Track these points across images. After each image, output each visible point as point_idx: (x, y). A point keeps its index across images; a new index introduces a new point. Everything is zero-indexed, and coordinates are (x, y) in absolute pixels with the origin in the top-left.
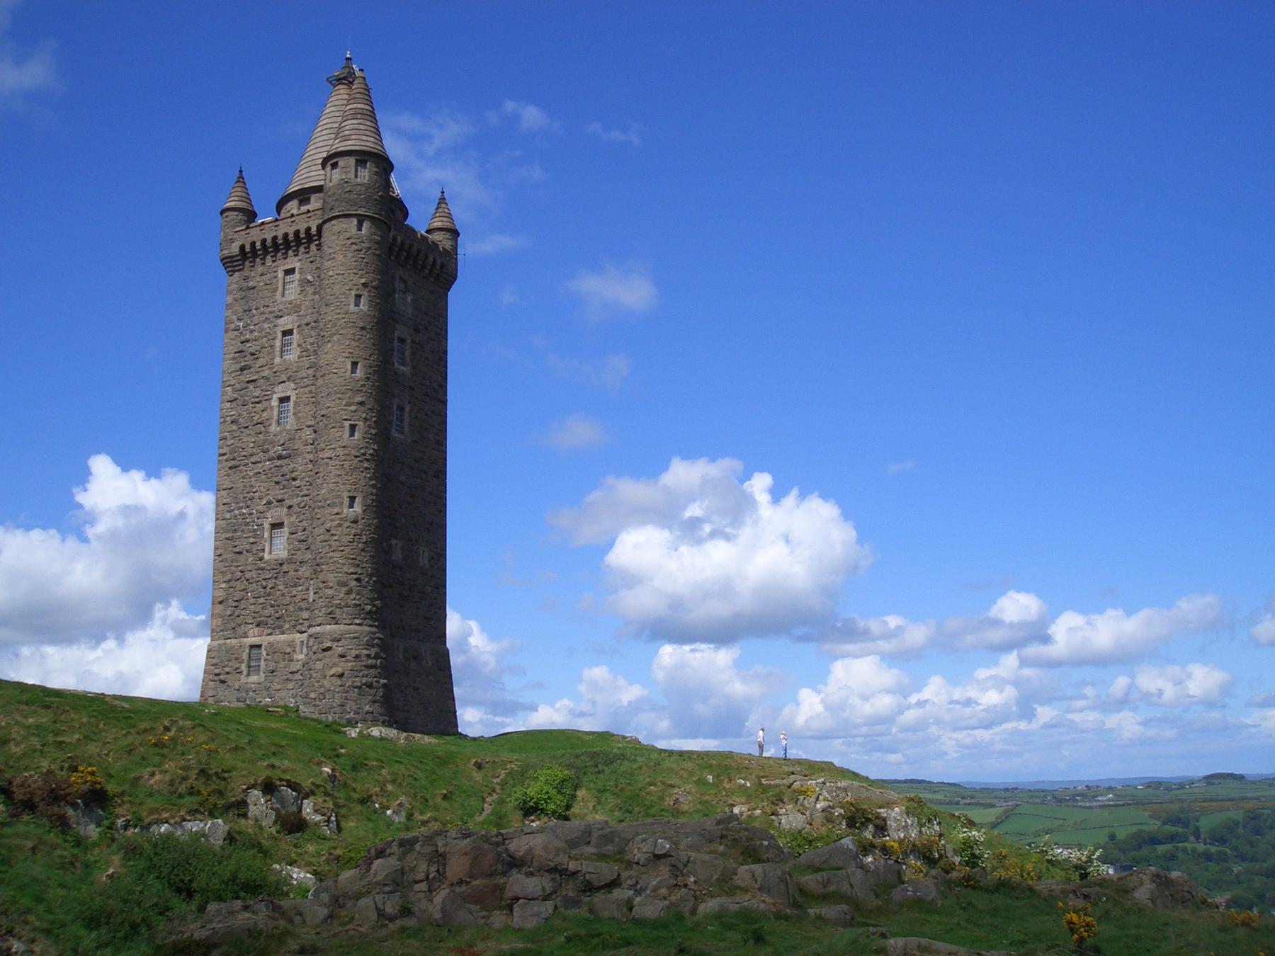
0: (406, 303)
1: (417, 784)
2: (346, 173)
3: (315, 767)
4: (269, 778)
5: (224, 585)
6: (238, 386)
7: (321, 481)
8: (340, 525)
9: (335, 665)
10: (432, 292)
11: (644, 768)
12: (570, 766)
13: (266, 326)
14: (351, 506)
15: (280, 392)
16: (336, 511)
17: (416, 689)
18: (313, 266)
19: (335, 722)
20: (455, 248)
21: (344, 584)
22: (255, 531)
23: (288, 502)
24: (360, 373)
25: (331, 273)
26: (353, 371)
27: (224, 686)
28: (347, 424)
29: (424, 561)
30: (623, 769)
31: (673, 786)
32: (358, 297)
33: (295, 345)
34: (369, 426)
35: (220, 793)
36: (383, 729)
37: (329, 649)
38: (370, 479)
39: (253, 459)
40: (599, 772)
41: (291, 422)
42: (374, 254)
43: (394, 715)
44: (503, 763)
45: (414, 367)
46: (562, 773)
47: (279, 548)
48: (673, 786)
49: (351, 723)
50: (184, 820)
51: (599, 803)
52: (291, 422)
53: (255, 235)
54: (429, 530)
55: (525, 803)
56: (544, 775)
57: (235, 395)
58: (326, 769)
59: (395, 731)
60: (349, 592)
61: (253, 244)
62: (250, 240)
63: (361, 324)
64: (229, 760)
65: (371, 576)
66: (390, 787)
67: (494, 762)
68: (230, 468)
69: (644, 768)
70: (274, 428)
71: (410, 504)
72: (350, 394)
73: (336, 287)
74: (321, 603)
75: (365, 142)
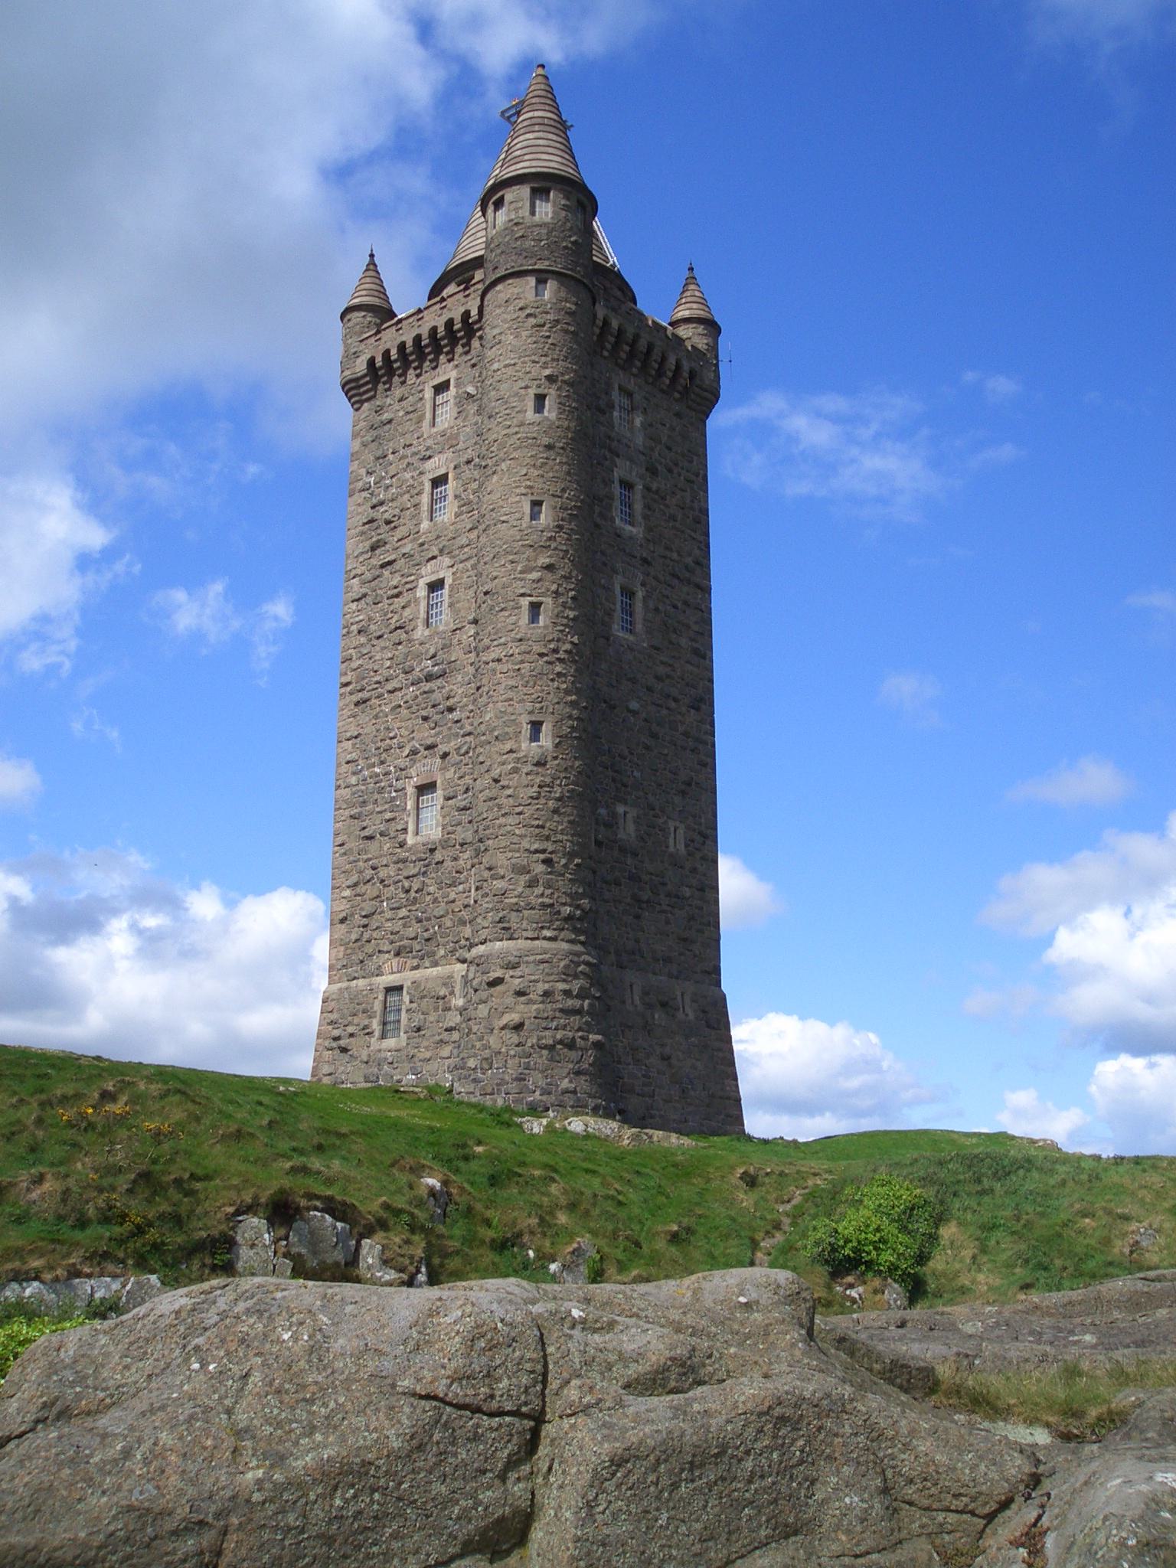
0: (632, 427)
1: (622, 1214)
2: (516, 210)
3: (403, 1178)
4: (282, 1191)
5: (347, 893)
6: (368, 576)
7: (484, 699)
8: (515, 770)
9: (509, 1009)
10: (678, 415)
11: (1071, 1184)
12: (926, 1181)
13: (407, 475)
14: (535, 736)
15: (429, 573)
16: (508, 747)
17: (666, 1058)
18: (476, 372)
19: (507, 1109)
20: (714, 348)
21: (524, 870)
22: (393, 799)
23: (442, 748)
24: (545, 518)
25: (496, 366)
26: (534, 516)
27: (345, 1057)
28: (525, 602)
29: (677, 844)
30: (1029, 1186)
31: (1126, 1218)
32: (540, 399)
33: (450, 498)
34: (564, 605)
35: (177, 1221)
36: (591, 1121)
37: (494, 983)
38: (567, 692)
39: (390, 686)
40: (983, 1193)
41: (445, 619)
42: (566, 332)
43: (614, 1095)
44: (801, 1176)
45: (649, 529)
46: (906, 1193)
47: (430, 823)
48: (1126, 1218)
49: (535, 1110)
50: (78, 1274)
51: (984, 1250)
52: (445, 619)
53: (390, 339)
54: (683, 793)
55: (834, 1249)
56: (874, 1196)
57: (364, 590)
58: (431, 1181)
59: (614, 1125)
60: (532, 884)
62: (382, 348)
63: (546, 441)
64: (215, 1155)
65: (571, 855)
66: (562, 1218)
67: (781, 1174)
68: (357, 704)
69: (1071, 1184)
70: (421, 632)
71: (647, 748)
72: (529, 552)
73: (504, 387)
74: (486, 904)
75: (550, 162)
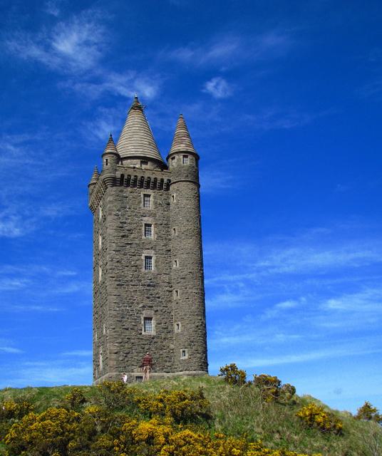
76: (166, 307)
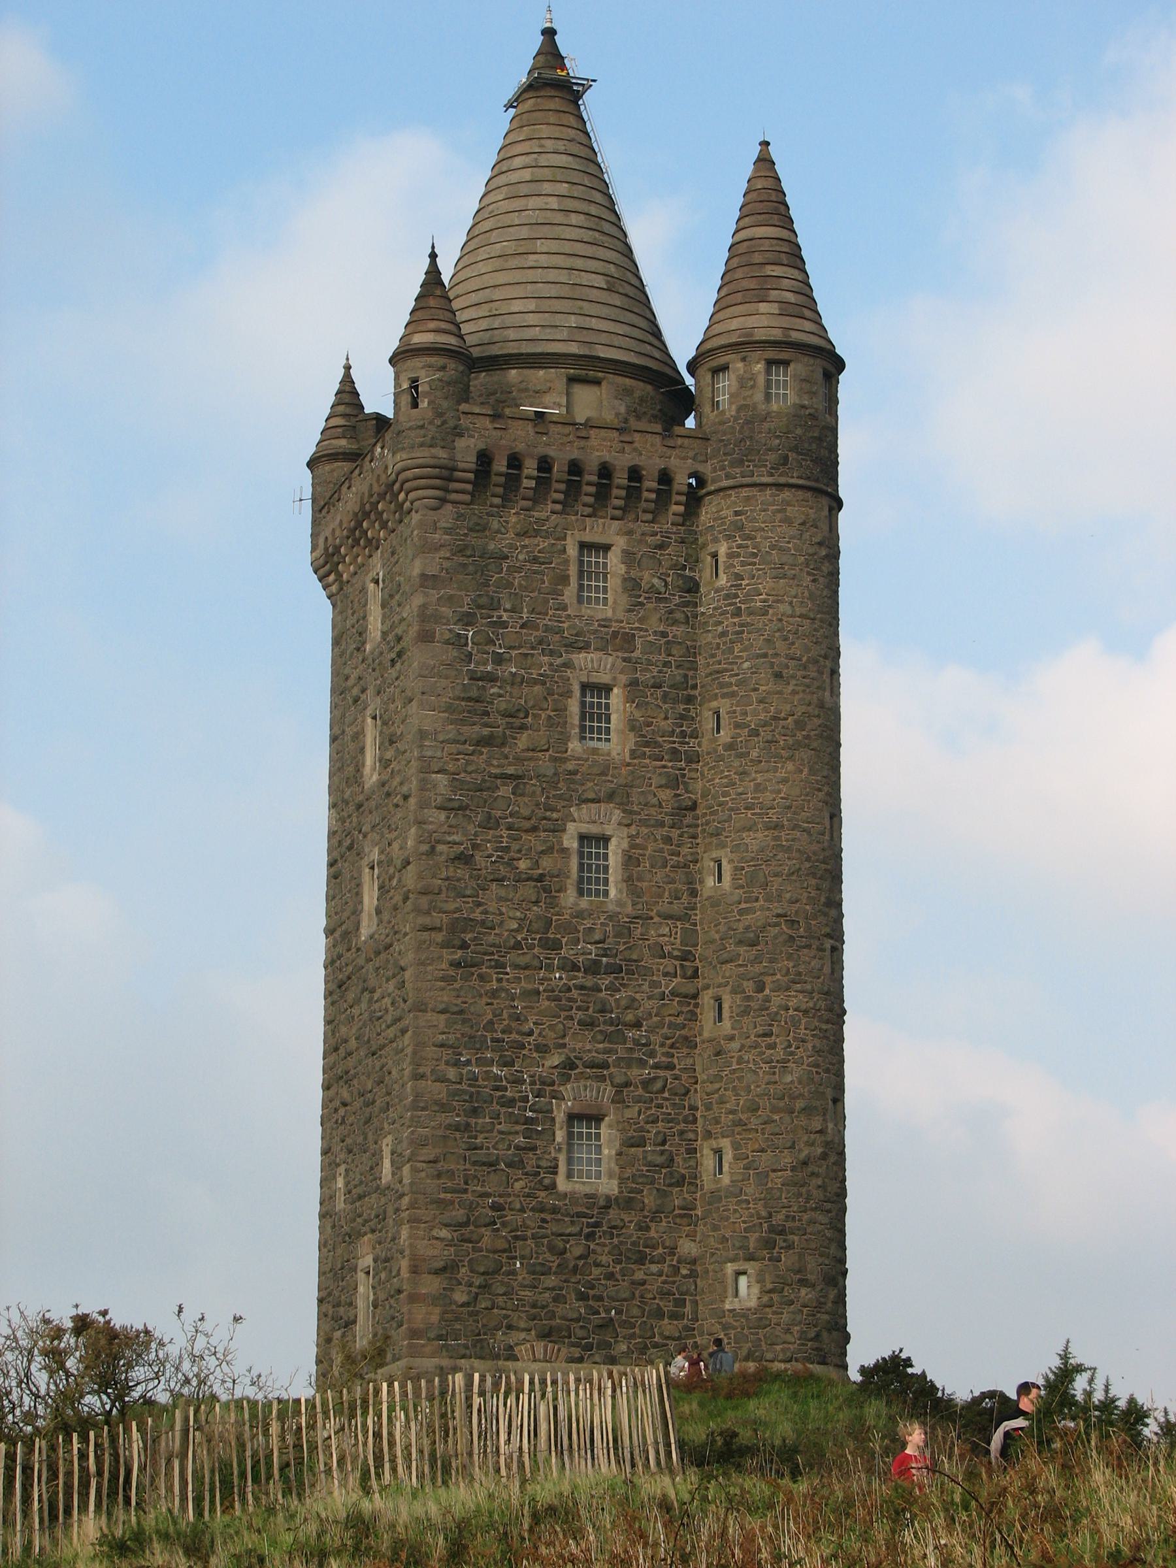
61: (515, 461)
76: (670, 1067)
